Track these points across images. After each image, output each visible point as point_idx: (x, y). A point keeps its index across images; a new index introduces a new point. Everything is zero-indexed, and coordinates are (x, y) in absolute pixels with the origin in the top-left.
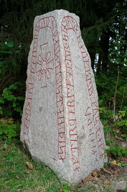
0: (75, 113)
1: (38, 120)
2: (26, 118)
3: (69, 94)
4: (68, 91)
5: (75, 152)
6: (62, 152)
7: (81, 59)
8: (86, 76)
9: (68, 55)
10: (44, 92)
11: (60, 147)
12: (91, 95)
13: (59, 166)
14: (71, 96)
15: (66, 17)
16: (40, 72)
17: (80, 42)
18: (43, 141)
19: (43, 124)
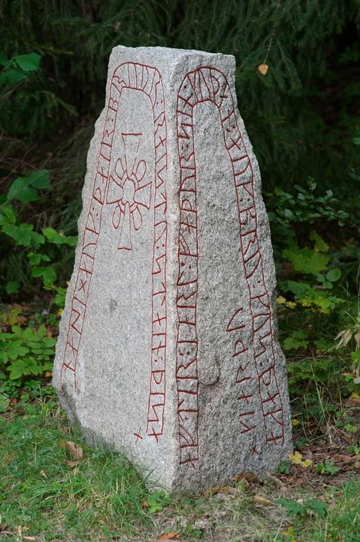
0: (198, 324)
1: (103, 334)
2: (71, 324)
3: (183, 277)
4: (181, 272)
5: (187, 419)
6: (156, 419)
7: (228, 180)
8: (241, 224)
9: (189, 177)
10: (125, 262)
11: (153, 407)
12: (251, 275)
13: (146, 452)
14: (188, 283)
15: (192, 72)
16: (116, 204)
17: (231, 128)
18: (115, 389)
19: (117, 345)
